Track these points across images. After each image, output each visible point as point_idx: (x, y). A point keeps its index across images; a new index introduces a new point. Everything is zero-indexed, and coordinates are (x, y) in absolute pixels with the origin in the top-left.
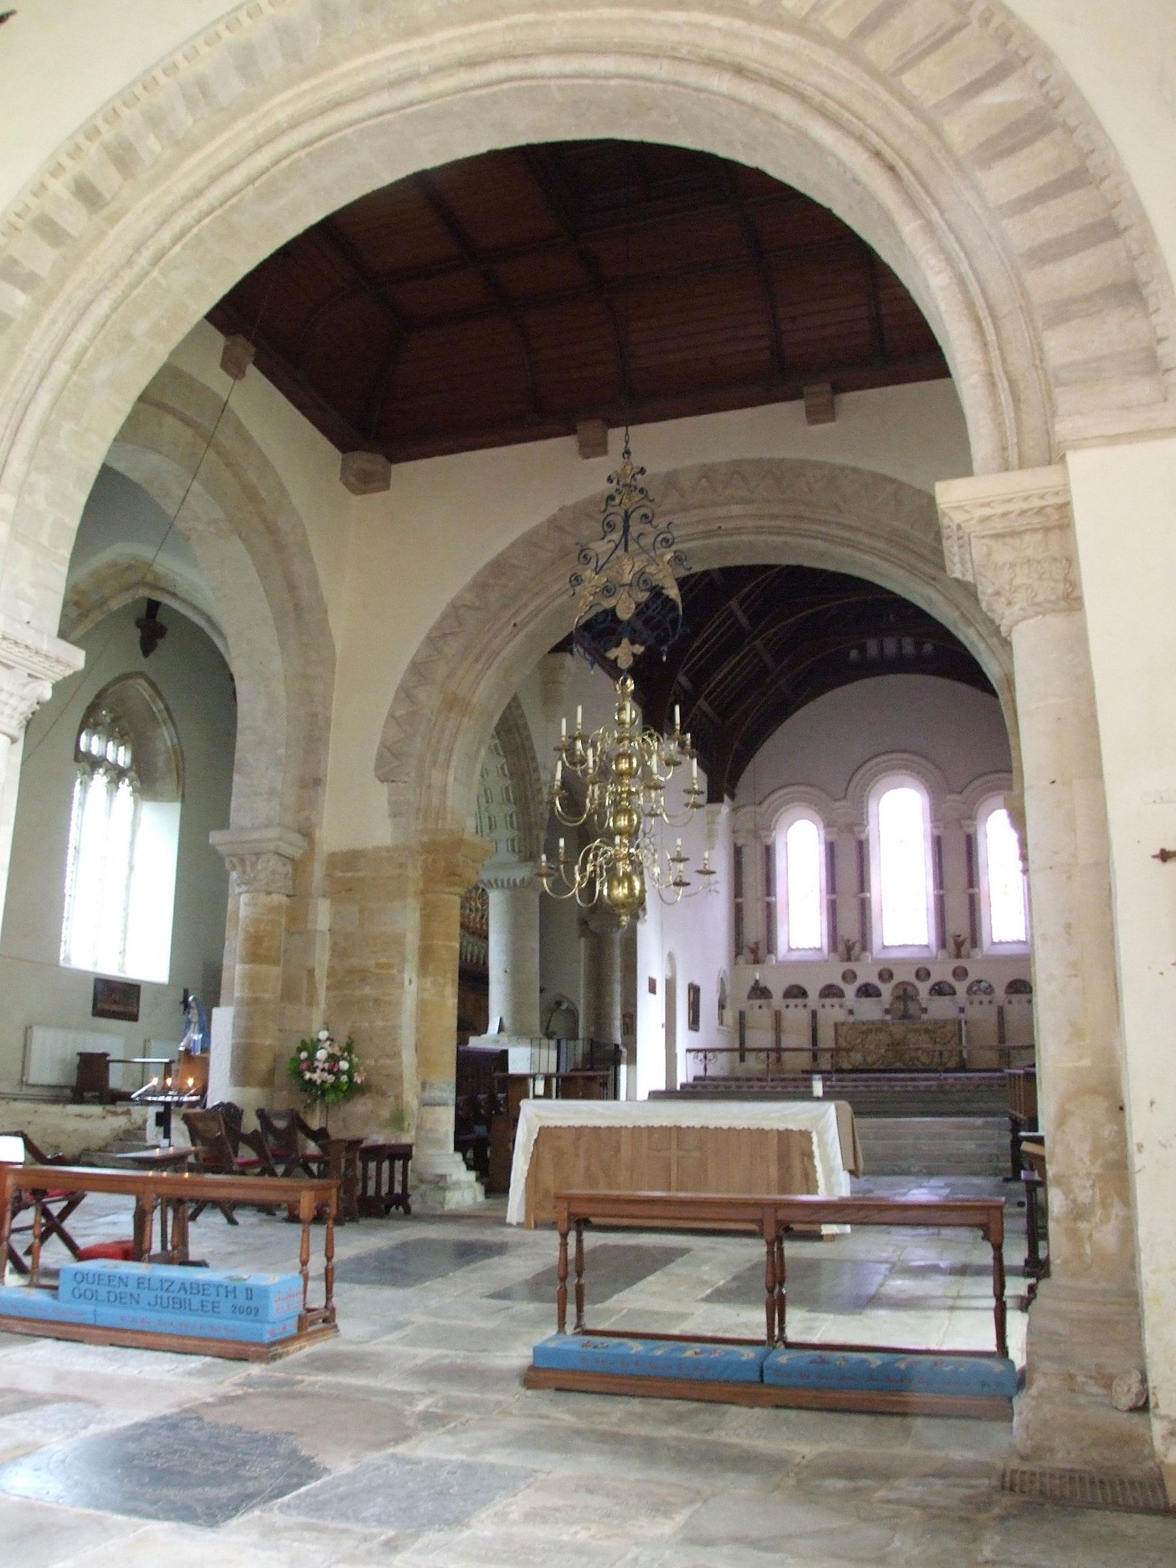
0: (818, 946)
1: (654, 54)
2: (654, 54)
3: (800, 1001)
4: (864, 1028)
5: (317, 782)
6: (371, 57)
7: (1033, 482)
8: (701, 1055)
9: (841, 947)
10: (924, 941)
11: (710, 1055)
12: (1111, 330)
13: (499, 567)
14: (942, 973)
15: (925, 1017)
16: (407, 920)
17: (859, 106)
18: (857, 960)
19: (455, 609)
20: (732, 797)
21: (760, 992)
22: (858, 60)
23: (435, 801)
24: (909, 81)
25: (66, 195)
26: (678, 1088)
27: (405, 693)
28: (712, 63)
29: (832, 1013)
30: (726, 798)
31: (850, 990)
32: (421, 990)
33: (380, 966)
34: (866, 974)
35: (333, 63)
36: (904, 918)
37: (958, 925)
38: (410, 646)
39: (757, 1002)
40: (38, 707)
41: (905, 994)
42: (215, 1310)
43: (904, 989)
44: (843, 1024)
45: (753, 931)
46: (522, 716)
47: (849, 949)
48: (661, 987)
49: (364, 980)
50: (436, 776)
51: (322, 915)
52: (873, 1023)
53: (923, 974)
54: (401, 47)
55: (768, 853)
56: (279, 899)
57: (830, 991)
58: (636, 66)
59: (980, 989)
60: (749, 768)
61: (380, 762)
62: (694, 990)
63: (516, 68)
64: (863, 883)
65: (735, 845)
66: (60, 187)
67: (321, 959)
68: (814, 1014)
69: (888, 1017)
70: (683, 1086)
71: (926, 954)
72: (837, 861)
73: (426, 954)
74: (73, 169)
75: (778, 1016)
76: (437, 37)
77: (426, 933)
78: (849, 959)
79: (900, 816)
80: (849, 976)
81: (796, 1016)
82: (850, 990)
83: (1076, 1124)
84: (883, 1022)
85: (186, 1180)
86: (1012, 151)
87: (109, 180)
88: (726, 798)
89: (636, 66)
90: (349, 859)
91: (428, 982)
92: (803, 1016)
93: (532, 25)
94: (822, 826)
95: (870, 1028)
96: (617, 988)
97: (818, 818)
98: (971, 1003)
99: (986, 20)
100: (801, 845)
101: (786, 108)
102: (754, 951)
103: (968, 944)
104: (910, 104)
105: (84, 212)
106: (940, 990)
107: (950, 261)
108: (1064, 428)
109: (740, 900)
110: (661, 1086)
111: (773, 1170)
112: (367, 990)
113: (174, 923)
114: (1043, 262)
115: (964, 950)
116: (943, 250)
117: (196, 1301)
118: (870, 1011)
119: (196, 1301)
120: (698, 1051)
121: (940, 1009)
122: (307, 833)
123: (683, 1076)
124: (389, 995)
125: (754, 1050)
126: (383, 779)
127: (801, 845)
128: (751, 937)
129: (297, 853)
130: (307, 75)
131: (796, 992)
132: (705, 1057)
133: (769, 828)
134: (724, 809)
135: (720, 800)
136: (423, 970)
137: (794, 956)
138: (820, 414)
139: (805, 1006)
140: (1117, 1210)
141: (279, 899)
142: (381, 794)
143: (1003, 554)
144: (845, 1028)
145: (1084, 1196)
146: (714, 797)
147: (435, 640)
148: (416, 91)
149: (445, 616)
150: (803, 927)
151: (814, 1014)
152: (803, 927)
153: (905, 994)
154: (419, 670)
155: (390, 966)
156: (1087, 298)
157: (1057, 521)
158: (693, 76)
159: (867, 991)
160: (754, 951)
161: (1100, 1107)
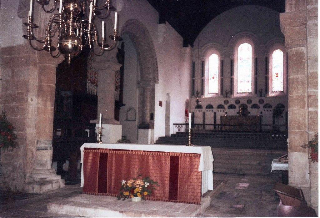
0: (217, 92)
3: (211, 110)
4: (230, 118)
8: (178, 126)
9: (224, 93)
10: (250, 91)
11: (180, 126)
14: (255, 101)
15: (249, 115)
18: (229, 97)
20: (192, 46)
26: (170, 136)
29: (221, 113)
30: (189, 46)
31: (226, 106)
33: (19, 94)
34: (232, 102)
36: (244, 84)
37: (261, 86)
39: (198, 110)
41: (244, 108)
43: (243, 105)
44: (223, 117)
46: (153, 45)
47: (261, 92)
48: (164, 104)
49: (13, 100)
52: (233, 116)
53: (249, 101)
55: (203, 64)
57: (220, 107)
60: (197, 40)
64: (232, 73)
65: (193, 61)
68: (215, 113)
69: (238, 115)
70: (172, 135)
71: (250, 95)
72: (224, 67)
73: (40, 90)
78: (227, 97)
79: (245, 53)
80: (226, 102)
81: (210, 115)
82: (226, 106)
84: (236, 116)
88: (189, 46)
94: (219, 55)
95: (232, 118)
96: (148, 104)
97: (218, 53)
98: (264, 111)
100: (213, 63)
103: (229, 93)
106: (255, 106)
109: (193, 78)
110: (163, 134)
112: (14, 104)
115: (228, 95)
118: (232, 112)
120: (177, 124)
121: (254, 112)
123: (173, 130)
124: (22, 105)
127: (213, 63)
128: (196, 88)
131: (210, 107)
132: (179, 126)
133: (204, 56)
134: (188, 49)
135: (187, 46)
139: (212, 111)
144: (224, 118)
146: (185, 45)
150: (212, 87)
151: (215, 113)
152: (212, 87)
153: (244, 108)
155: (22, 94)
159: (231, 107)
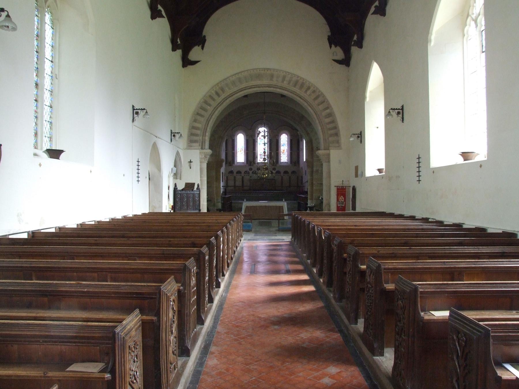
25: (214, 94)
29: (247, 177)
31: (251, 172)
34: (254, 168)
40: (333, 46)
45: (230, 159)
57: (246, 172)
59: (278, 172)
75: (235, 177)
80: (251, 169)
81: (239, 177)
82: (251, 172)
85: (209, 258)
92: (241, 177)
102: (230, 163)
113: (487, 103)
125: (235, 183)
131: (239, 172)
137: (239, 164)
157: (329, 155)
160: (230, 163)
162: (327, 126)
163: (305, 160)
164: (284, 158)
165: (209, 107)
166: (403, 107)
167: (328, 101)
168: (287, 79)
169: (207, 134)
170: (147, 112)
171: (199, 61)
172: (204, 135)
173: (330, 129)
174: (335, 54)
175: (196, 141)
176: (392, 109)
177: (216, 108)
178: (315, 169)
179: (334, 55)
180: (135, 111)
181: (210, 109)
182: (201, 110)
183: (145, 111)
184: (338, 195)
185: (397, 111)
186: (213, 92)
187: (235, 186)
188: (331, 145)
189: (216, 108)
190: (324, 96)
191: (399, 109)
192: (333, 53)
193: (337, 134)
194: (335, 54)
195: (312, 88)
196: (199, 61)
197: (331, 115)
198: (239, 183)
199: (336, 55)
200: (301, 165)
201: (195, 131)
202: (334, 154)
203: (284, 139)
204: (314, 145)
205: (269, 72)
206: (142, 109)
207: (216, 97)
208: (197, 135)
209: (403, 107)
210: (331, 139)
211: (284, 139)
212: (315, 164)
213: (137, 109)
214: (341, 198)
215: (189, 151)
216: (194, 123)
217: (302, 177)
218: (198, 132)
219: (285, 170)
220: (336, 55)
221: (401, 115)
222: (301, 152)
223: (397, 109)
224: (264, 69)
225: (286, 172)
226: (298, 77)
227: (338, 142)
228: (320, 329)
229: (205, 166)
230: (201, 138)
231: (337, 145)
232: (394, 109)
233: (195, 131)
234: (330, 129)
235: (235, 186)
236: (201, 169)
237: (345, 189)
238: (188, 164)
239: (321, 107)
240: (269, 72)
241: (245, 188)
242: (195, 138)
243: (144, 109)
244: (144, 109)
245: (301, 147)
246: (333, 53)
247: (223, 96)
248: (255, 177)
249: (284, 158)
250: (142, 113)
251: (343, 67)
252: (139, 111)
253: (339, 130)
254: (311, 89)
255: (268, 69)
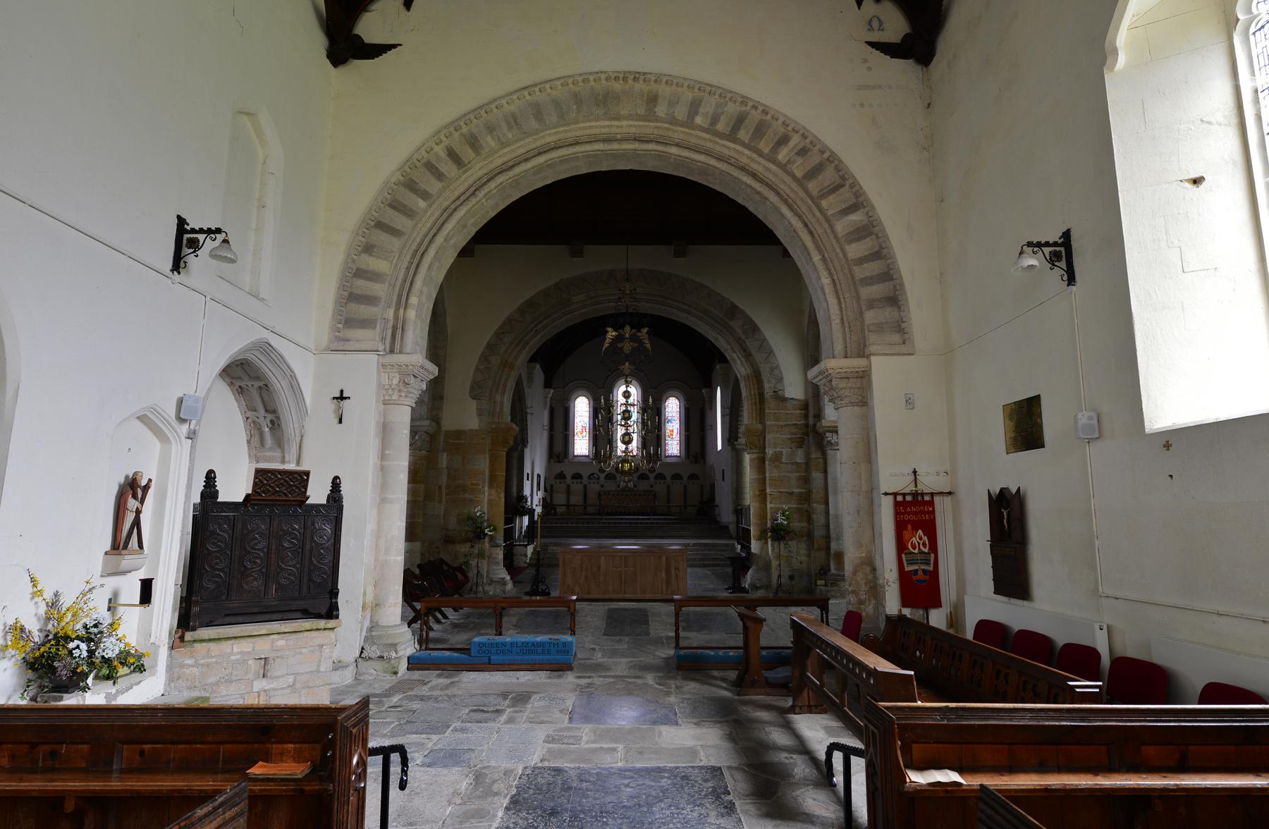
1: (720, 159)
2: (720, 159)
5: (441, 398)
6: (593, 124)
7: (858, 363)
12: (888, 313)
13: (530, 303)
16: (482, 464)
17: (799, 203)
19: (509, 322)
21: (561, 476)
22: (774, 162)
23: (498, 409)
24: (824, 203)
25: (443, 155)
27: (484, 358)
28: (743, 169)
29: (594, 488)
32: (490, 495)
35: (577, 122)
38: (488, 336)
42: (549, 652)
45: (558, 448)
50: (498, 398)
51: (444, 460)
54: (608, 123)
56: (424, 452)
58: (713, 162)
59: (660, 476)
61: (472, 388)
62: (539, 476)
63: (660, 148)
66: (440, 150)
67: (444, 480)
73: (493, 478)
74: (446, 142)
76: (625, 123)
77: (492, 469)
81: (577, 487)
83: (859, 577)
86: (858, 240)
87: (467, 153)
89: (713, 162)
90: (458, 434)
91: (493, 492)
92: (580, 487)
93: (667, 129)
96: (515, 479)
99: (852, 186)
100: (582, 408)
101: (773, 198)
104: (821, 210)
105: (455, 167)
107: (830, 274)
108: (873, 349)
111: (664, 575)
112: (467, 496)
114: (867, 285)
116: (828, 269)
117: (540, 650)
119: (540, 650)
122: (436, 420)
126: (474, 397)
129: (431, 431)
130: (566, 125)
131: (577, 476)
136: (491, 486)
138: (680, 253)
140: (873, 602)
141: (424, 452)
142: (472, 405)
143: (842, 384)
145: (863, 597)
147: (499, 334)
148: (615, 146)
149: (504, 324)
154: (491, 348)
156: (879, 300)
157: (864, 376)
158: (736, 173)
160: (558, 457)
161: (868, 569)
162: (856, 269)
163: (719, 448)
164: (673, 446)
165: (422, 204)
166: (1067, 235)
167: (855, 184)
168: (708, 107)
169: (414, 300)
170: (225, 241)
171: (394, 46)
172: (402, 302)
173: (868, 281)
174: (875, 24)
175: (366, 323)
176: (1030, 244)
177: (449, 212)
178: (770, 452)
179: (871, 29)
180: (186, 236)
181: (428, 213)
182: (390, 211)
183: (220, 237)
184: (900, 527)
185: (1047, 250)
186: (437, 149)
187: (568, 505)
188: (872, 338)
189: (449, 212)
190: (840, 168)
191: (1055, 244)
192: (870, 23)
193: (894, 300)
194: (875, 24)
195: (795, 140)
196: (394, 46)
197: (869, 229)
198: (576, 499)
199: (881, 29)
200: (711, 459)
201: (362, 286)
202: (887, 372)
203: (673, 407)
204: (766, 385)
205: (640, 86)
206: (209, 231)
207: (448, 168)
208: (370, 300)
209: (1067, 235)
210: (870, 317)
211: (673, 407)
212: (769, 437)
213: (193, 231)
214: (918, 539)
215: (339, 357)
216: (365, 257)
217: (712, 486)
218: (378, 289)
219: (675, 471)
220: (881, 29)
221: (1063, 264)
222: (709, 433)
223: (1047, 244)
224: (624, 77)
225: (677, 477)
226: (745, 100)
227: (900, 328)
228: (693, 680)
229: (402, 417)
230: (391, 312)
231: (896, 338)
232: (1039, 245)
233: (362, 286)
234: (868, 281)
235: (568, 505)
236: (385, 430)
237: (931, 503)
238: (331, 406)
239: (831, 204)
240: (640, 86)
241: (590, 509)
242: (364, 311)
243: (218, 231)
244: (218, 231)
245: (708, 422)
246: (870, 23)
247: (477, 170)
248: (610, 486)
249: (673, 446)
250: (209, 245)
251: (902, 69)
252: (201, 237)
253: (902, 285)
254: (792, 143)
255: (637, 76)
